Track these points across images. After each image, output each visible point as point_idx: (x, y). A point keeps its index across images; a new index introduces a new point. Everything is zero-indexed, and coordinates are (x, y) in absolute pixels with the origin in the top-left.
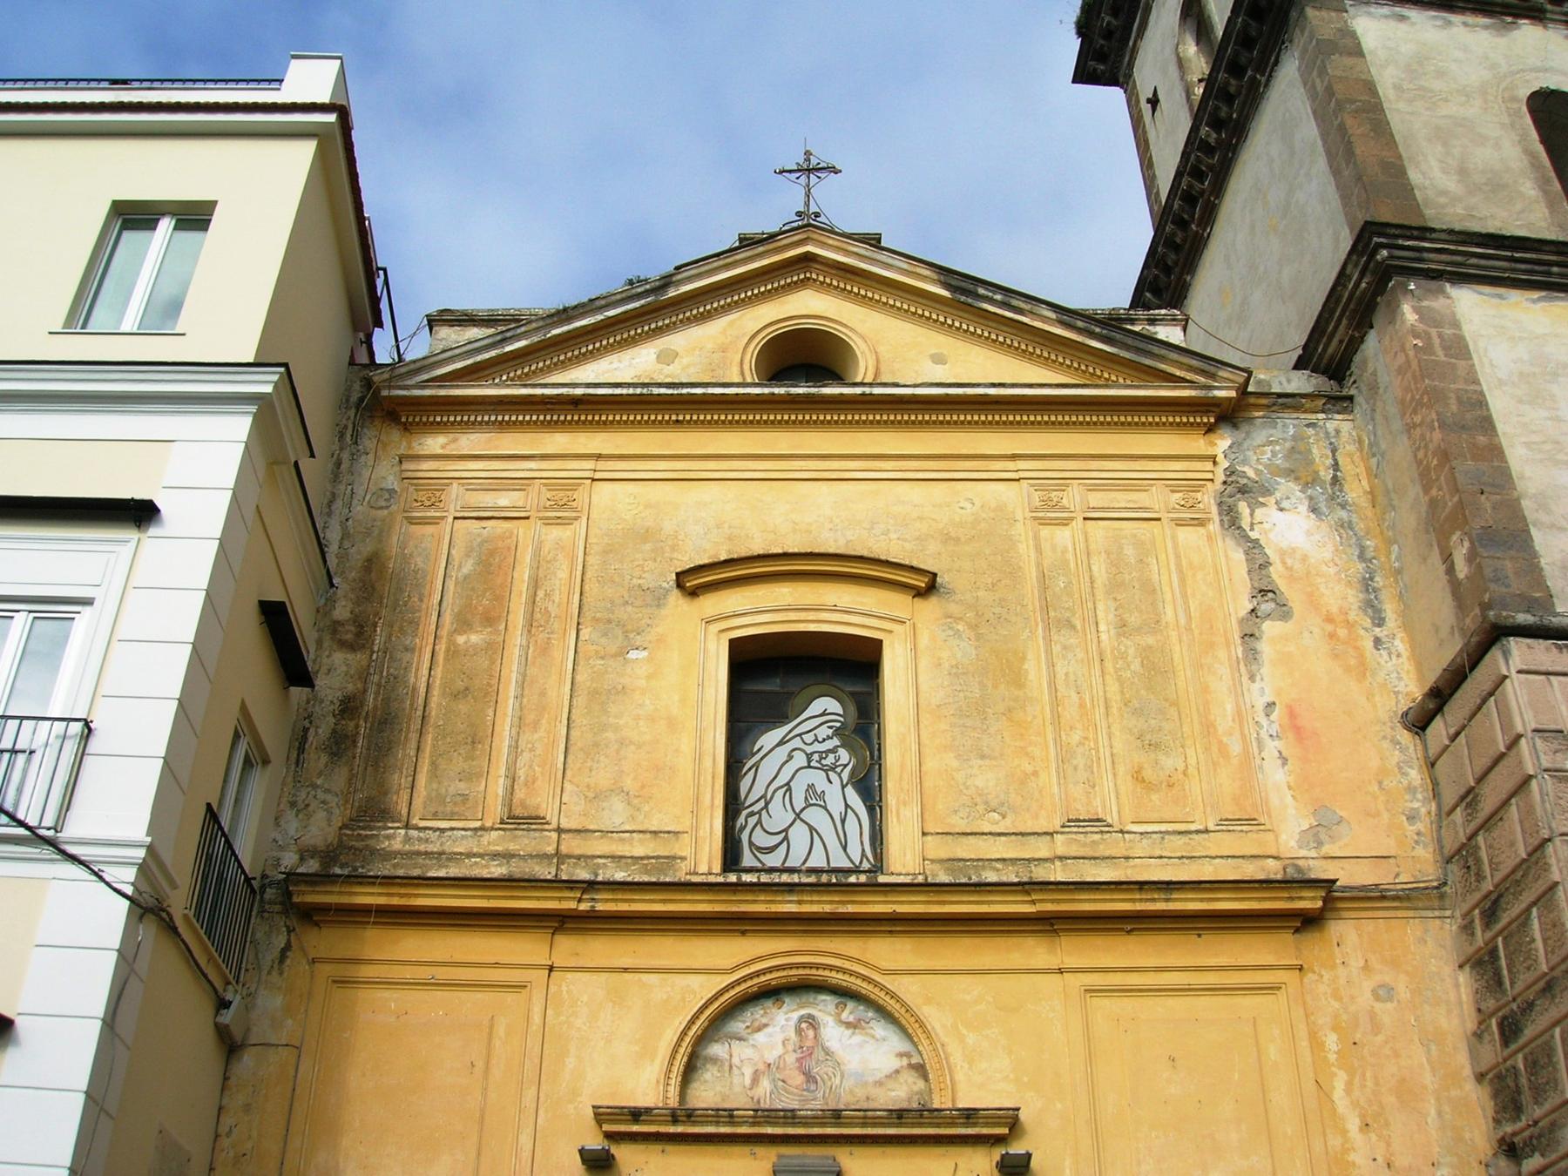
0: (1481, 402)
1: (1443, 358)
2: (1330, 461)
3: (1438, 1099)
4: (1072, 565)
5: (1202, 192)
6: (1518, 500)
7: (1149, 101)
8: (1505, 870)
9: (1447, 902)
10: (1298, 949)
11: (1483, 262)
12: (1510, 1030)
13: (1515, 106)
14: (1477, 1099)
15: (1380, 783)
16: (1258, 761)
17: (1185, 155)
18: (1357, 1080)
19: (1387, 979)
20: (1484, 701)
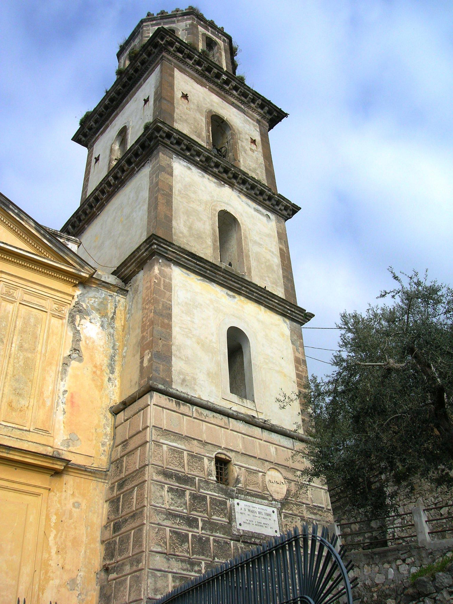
0: (170, 308)
1: (162, 289)
2: (113, 311)
3: (86, 547)
4: (10, 319)
5: (102, 199)
6: (171, 345)
7: (95, 158)
8: (130, 471)
9: (108, 477)
10: (50, 482)
11: (186, 261)
12: (117, 527)
13: (214, 212)
14: (99, 549)
15: (96, 429)
16: (55, 411)
17: (101, 184)
18: (59, 534)
19: (80, 500)
20: (140, 411)
